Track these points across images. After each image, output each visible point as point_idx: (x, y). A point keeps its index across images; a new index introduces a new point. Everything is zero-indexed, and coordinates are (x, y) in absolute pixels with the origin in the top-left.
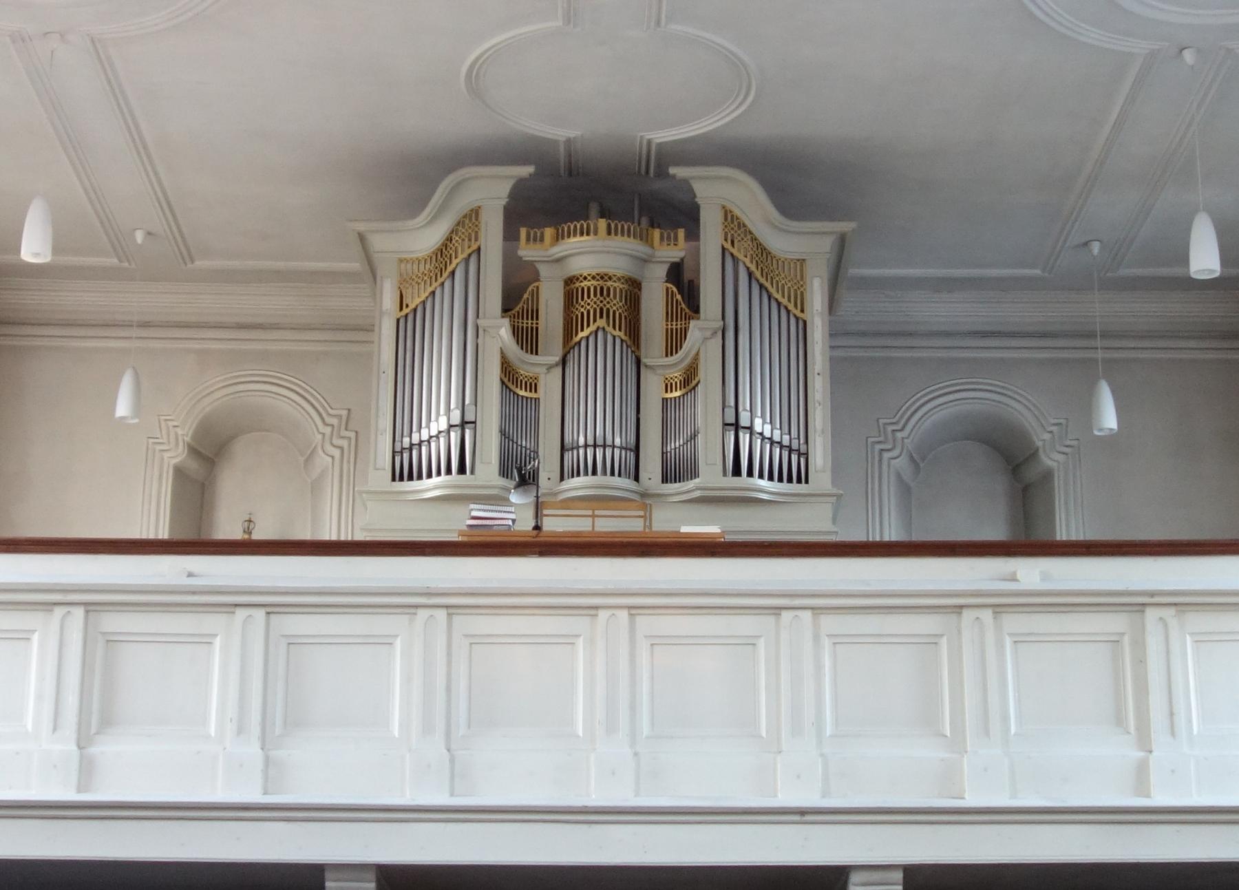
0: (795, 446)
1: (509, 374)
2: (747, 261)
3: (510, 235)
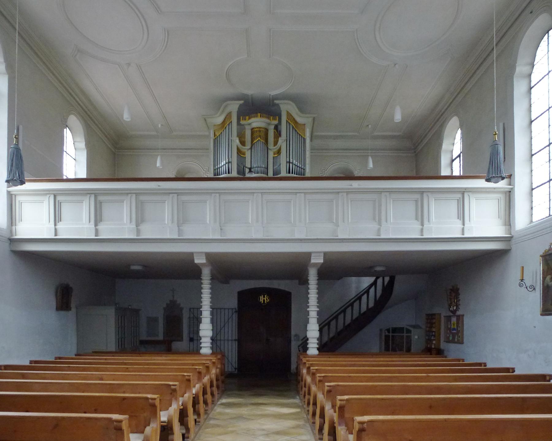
0: (302, 167)
1: (239, 152)
2: (292, 124)
3: (239, 120)
